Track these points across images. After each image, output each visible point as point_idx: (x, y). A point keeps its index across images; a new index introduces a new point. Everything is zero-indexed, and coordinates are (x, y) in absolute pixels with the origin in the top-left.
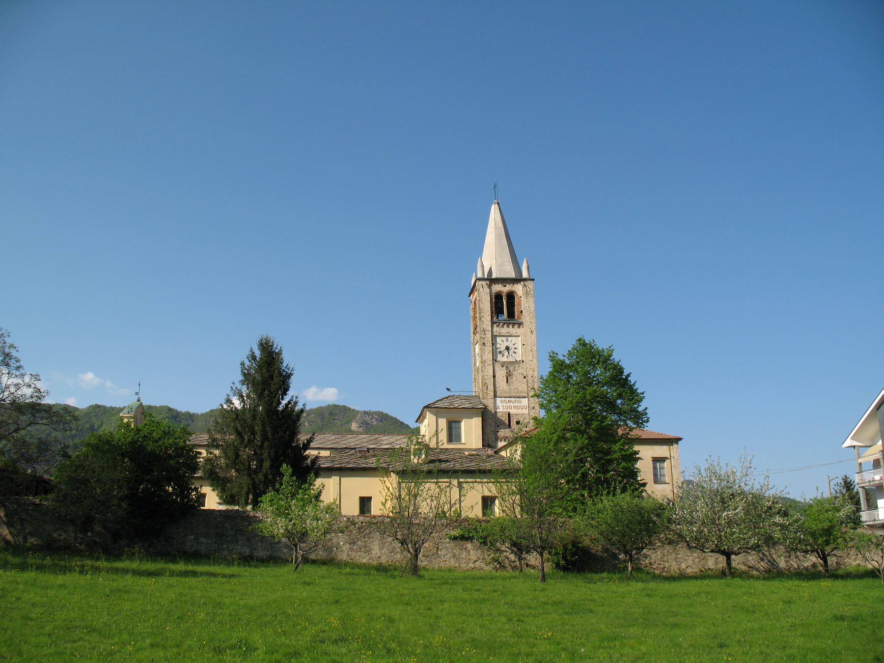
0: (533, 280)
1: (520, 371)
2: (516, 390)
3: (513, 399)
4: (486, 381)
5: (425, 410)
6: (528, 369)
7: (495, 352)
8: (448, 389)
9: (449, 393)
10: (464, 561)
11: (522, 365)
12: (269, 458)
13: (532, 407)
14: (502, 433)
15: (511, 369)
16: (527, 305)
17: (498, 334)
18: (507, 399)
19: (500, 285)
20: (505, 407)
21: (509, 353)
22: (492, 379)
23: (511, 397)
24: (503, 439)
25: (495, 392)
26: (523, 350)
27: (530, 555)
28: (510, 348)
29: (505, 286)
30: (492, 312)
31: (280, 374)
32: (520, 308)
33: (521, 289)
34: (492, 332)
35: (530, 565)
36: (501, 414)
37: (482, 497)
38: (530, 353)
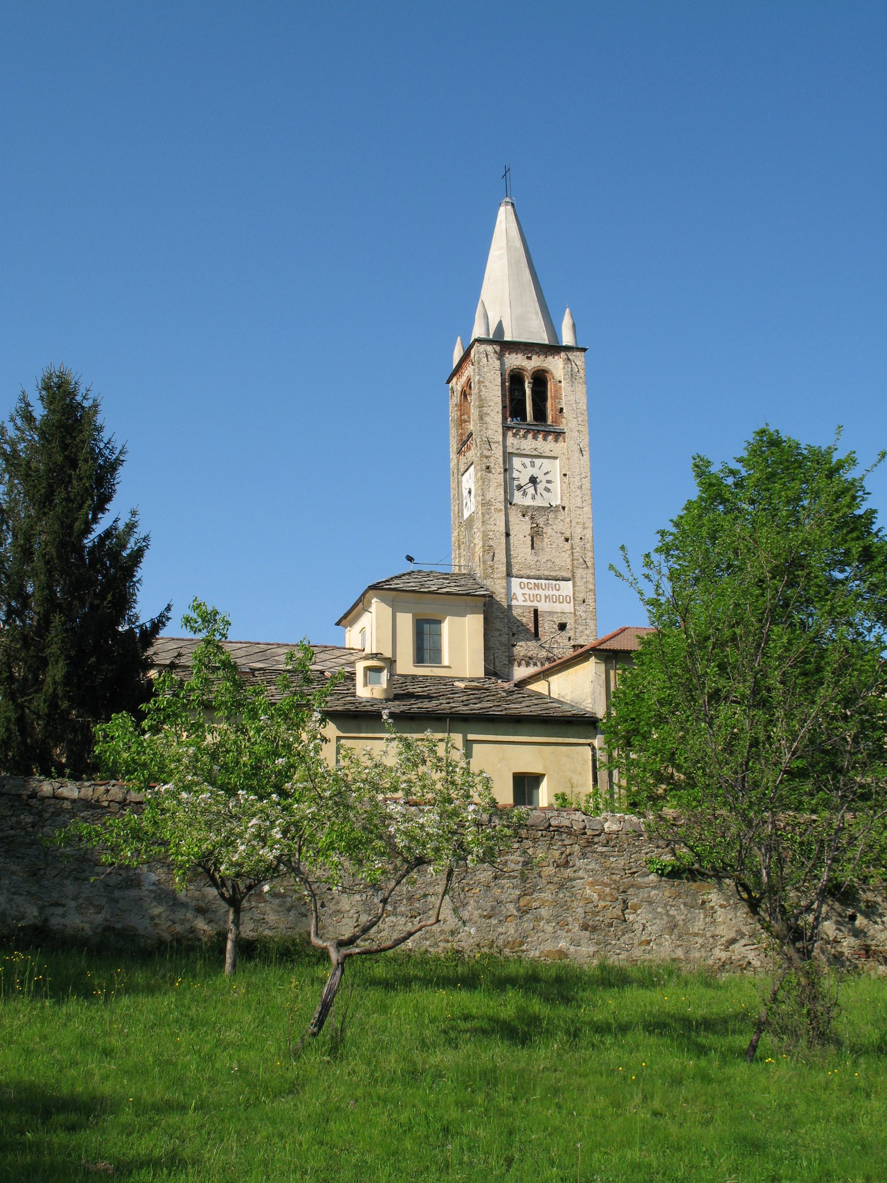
0: (584, 350)
1: (559, 526)
2: (550, 564)
3: (543, 582)
4: (491, 543)
5: (371, 592)
6: (574, 524)
7: (509, 486)
8: (410, 559)
9: (411, 567)
10: (700, 940)
11: (561, 515)
12: (63, 657)
13: (581, 599)
14: (522, 648)
15: (541, 521)
16: (572, 398)
17: (516, 452)
18: (532, 581)
19: (520, 356)
20: (527, 597)
21: (536, 490)
22: (503, 539)
23: (539, 578)
24: (523, 662)
25: (509, 565)
26: (565, 485)
27: (876, 922)
28: (538, 480)
29: (529, 358)
30: (504, 407)
31: (94, 455)
32: (559, 403)
33: (562, 366)
34: (505, 447)
35: (875, 952)
36: (520, 611)
37: (514, 774)
38: (579, 491)
